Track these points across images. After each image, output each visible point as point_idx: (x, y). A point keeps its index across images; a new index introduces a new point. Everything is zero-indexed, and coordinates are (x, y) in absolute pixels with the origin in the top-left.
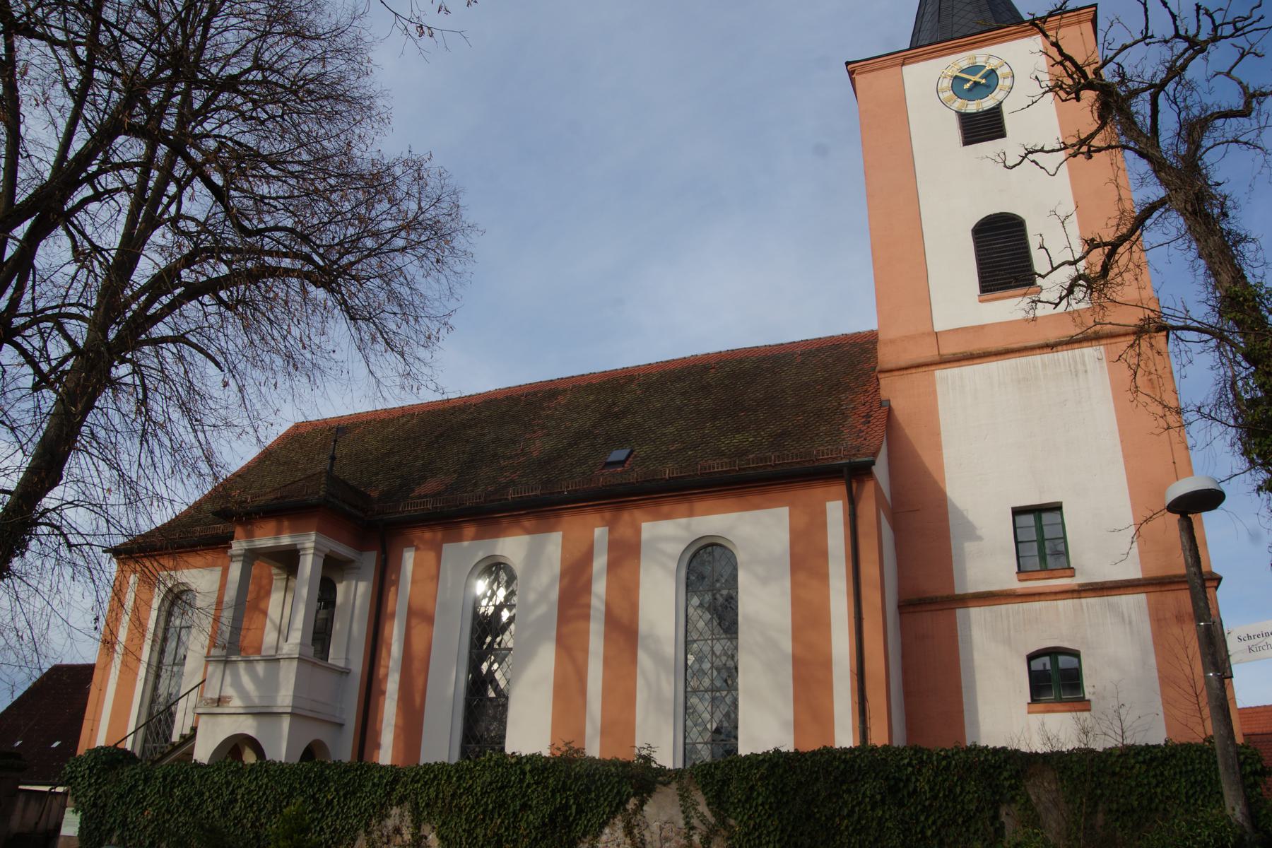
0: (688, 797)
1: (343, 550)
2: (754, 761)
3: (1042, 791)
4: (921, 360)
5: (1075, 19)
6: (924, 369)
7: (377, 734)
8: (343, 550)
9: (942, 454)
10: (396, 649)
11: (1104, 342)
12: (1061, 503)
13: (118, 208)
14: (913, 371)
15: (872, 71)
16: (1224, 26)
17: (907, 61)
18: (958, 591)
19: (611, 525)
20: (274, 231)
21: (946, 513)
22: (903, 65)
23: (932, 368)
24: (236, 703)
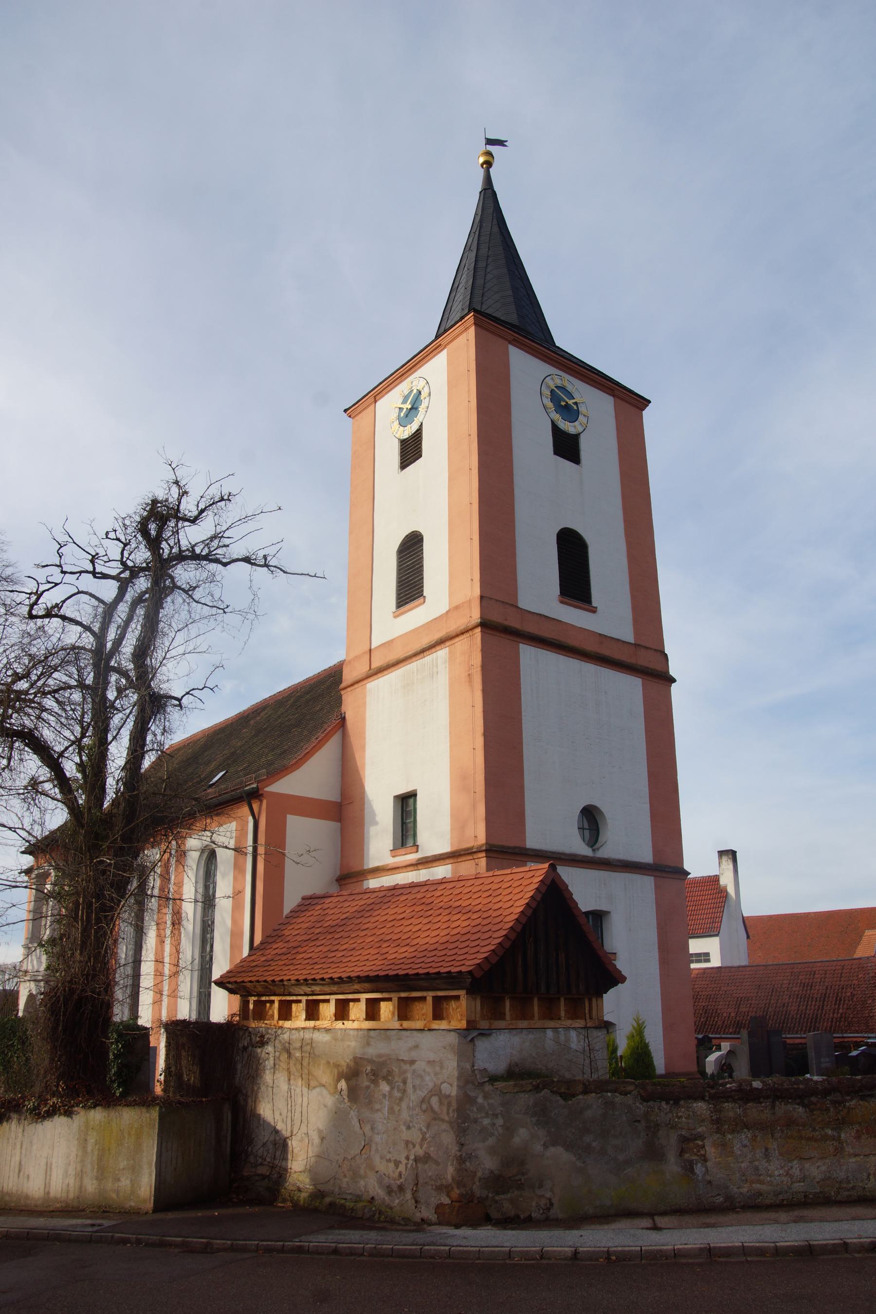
0: (262, 1036)
4: (360, 677)
6: (360, 684)
11: (448, 644)
12: (416, 790)
13: (90, 557)
14: (356, 686)
16: (197, 600)
18: (365, 867)
20: (201, 514)
21: (363, 804)
22: (376, 402)
23: (365, 682)
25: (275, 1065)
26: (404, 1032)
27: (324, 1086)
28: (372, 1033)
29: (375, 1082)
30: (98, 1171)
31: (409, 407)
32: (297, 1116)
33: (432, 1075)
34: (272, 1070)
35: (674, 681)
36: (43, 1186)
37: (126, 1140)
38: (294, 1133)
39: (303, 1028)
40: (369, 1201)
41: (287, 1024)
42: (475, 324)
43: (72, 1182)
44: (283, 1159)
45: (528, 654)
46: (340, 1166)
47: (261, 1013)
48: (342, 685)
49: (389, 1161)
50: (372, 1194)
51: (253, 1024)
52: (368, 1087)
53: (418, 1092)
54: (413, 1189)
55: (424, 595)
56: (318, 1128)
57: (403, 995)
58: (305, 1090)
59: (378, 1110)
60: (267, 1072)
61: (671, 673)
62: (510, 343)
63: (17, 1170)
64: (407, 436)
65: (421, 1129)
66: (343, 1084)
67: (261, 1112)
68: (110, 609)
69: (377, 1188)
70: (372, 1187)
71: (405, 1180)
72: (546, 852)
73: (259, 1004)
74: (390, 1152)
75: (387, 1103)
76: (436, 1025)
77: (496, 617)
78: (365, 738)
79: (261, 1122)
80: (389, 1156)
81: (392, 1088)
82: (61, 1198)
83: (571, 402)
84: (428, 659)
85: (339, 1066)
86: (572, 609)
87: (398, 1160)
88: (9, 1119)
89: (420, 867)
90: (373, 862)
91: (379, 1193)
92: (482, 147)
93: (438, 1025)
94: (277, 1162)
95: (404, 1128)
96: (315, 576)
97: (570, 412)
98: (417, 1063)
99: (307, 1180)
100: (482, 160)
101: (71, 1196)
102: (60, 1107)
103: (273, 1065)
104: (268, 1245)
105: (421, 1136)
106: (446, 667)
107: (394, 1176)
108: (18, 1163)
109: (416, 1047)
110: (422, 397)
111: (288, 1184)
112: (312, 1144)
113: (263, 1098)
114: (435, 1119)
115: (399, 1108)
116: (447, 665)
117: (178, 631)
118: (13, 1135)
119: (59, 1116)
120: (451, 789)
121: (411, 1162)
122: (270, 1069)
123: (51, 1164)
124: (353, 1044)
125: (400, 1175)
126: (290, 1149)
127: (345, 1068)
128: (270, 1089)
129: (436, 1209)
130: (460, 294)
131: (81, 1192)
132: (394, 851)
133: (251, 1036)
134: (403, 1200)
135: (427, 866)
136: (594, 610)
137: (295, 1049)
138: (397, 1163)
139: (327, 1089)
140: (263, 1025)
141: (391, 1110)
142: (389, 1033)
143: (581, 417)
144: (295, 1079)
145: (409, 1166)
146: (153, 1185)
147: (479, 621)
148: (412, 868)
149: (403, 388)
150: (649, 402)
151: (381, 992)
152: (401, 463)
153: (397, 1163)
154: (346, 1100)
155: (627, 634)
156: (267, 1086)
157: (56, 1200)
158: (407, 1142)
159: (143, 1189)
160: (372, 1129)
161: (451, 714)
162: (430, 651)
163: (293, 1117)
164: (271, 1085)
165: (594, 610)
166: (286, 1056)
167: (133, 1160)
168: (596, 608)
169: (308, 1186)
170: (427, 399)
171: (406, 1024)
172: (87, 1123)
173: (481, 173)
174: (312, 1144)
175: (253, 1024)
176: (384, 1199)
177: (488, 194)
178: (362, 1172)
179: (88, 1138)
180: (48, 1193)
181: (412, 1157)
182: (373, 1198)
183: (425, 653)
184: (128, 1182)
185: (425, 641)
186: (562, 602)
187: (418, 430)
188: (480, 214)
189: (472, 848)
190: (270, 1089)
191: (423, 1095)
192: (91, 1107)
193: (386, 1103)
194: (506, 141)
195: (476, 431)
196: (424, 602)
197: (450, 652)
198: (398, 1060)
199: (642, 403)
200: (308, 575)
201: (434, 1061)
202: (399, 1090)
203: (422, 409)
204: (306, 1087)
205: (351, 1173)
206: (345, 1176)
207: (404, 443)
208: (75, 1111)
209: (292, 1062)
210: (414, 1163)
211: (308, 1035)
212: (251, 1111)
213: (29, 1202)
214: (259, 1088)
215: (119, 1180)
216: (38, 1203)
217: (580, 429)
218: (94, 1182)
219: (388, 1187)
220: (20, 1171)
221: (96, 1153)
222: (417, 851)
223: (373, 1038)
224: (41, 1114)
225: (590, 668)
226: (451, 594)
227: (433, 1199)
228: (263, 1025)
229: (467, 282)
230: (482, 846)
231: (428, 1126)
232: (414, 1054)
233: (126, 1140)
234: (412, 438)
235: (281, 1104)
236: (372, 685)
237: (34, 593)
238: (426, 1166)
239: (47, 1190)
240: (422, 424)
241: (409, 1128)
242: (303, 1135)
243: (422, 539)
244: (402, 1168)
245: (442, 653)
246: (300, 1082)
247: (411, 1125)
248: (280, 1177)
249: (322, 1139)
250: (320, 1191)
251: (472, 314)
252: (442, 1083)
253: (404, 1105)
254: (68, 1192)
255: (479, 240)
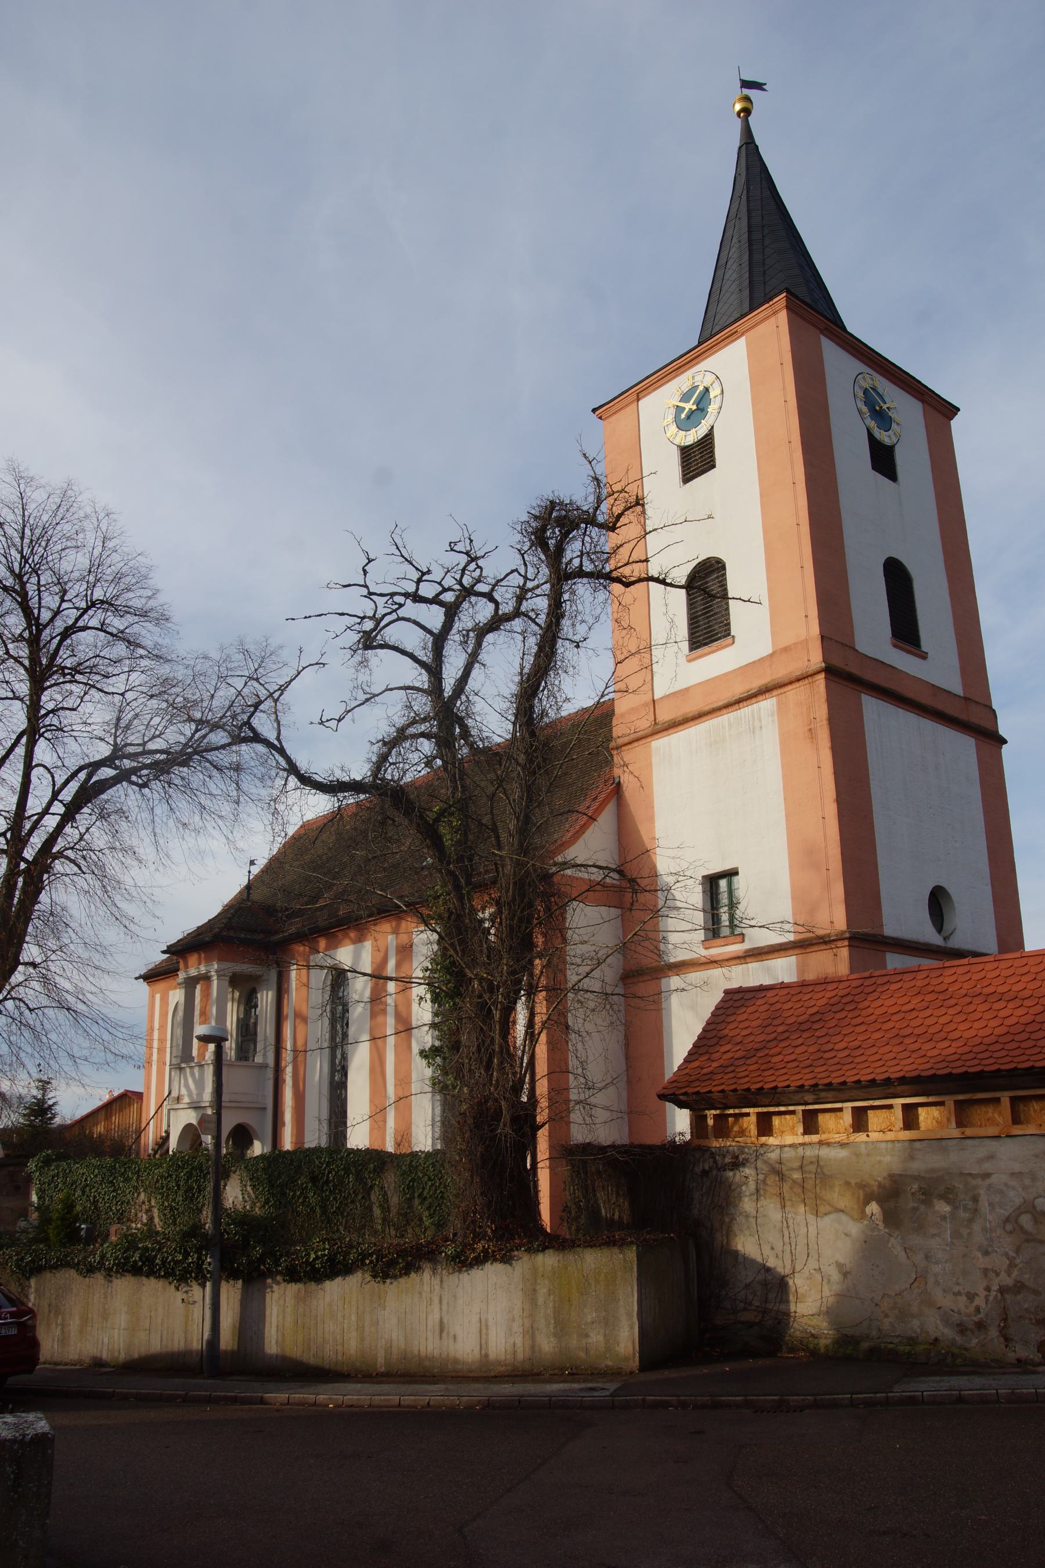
1: (244, 968)
2: (352, 1151)
3: (390, 1179)
5: (770, 310)
7: (283, 1114)
8: (244, 968)
9: (654, 827)
10: (289, 1045)
11: (775, 693)
14: (636, 744)
15: (615, 413)
17: (641, 395)
19: (396, 932)
22: (638, 400)
23: (649, 739)
24: (186, 1100)
25: (757, 1190)
26: (968, 1141)
27: (843, 1211)
28: (917, 1145)
29: (927, 1202)
30: (555, 1327)
31: (694, 407)
32: (801, 1249)
33: (1020, 1189)
34: (755, 1197)
35: (1005, 742)
36: (478, 1347)
37: (593, 1287)
38: (798, 1269)
39: (803, 1144)
40: (932, 1344)
41: (771, 1141)
42: (787, 307)
43: (519, 1341)
44: (781, 1301)
45: (872, 707)
46: (877, 1305)
47: (722, 1129)
48: (612, 744)
49: (959, 1293)
50: (933, 1334)
51: (716, 1144)
52: (915, 1209)
53: (998, 1210)
54: (999, 1325)
55: (732, 634)
56: (837, 1262)
57: (960, 1097)
58: (811, 1218)
59: (934, 1235)
60: (746, 1199)
61: (1001, 732)
62: (822, 332)
63: (437, 1329)
64: (691, 443)
65: (1006, 1255)
66: (873, 1208)
67: (740, 1247)
68: (439, 640)
69: (941, 1328)
70: (933, 1326)
71: (987, 1315)
72: (909, 941)
73: (720, 1119)
74: (958, 1284)
75: (949, 1225)
76: (1017, 1130)
77: (838, 662)
78: (653, 807)
79: (740, 1259)
80: (956, 1289)
81: (956, 1208)
82: (505, 1360)
83: (885, 407)
84: (746, 711)
85: (865, 1186)
86: (904, 654)
87: (972, 1292)
88: (418, 1269)
89: (748, 960)
90: (677, 956)
91: (948, 1333)
92: (737, 91)
93: (1022, 1130)
94: (770, 1306)
95: (979, 1255)
96: (749, 601)
97: (882, 417)
98: (994, 1176)
99: (825, 1324)
100: (738, 107)
101: (520, 1356)
102: (493, 1251)
103: (755, 1191)
104: (865, 1398)
105: (1008, 1262)
106: (773, 721)
107: (968, 1311)
108: (437, 1321)
109: (991, 1157)
110: (712, 395)
111: (792, 1330)
112: (829, 1281)
113: (741, 1230)
114: (1028, 1241)
115: (969, 1231)
116: (776, 718)
117: (619, 663)
118: (426, 1288)
119: (492, 1263)
120: (791, 867)
121: (993, 1294)
122: (751, 1195)
123: (487, 1321)
124: (887, 1159)
125: (978, 1310)
126: (793, 1289)
127: (875, 1188)
128: (752, 1220)
129: (1038, 1348)
130: (730, 272)
131: (533, 1352)
132: (706, 943)
133: (714, 1158)
134: (984, 1338)
135: (760, 958)
136: (924, 656)
137: (792, 1169)
138: (971, 1297)
139: (847, 1214)
140: (734, 1144)
141: (956, 1234)
142: (944, 1142)
143: (894, 426)
144: (792, 1206)
145: (991, 1298)
146: (637, 1339)
147: (823, 665)
148: (738, 961)
149: (682, 382)
150: (958, 410)
151: (928, 1095)
152: (684, 475)
153: (971, 1297)
154: (881, 1226)
155: (954, 684)
156: (747, 1216)
157: (499, 1363)
158: (985, 1271)
159: (622, 1345)
160: (927, 1257)
161: (784, 776)
162: (749, 702)
163: (794, 1251)
164: (754, 1213)
165: (924, 656)
166: (777, 1179)
167: (606, 1311)
168: (927, 653)
169: (826, 1332)
170: (719, 398)
171: (969, 1132)
172: (534, 1270)
173: (738, 124)
174: (829, 1281)
175: (716, 1144)
176: (954, 1339)
177: (749, 149)
178: (915, 1309)
179: (538, 1287)
180: (487, 1355)
181: (995, 1288)
182: (936, 1340)
183: (741, 704)
184: (601, 1338)
185: (739, 690)
186: (895, 646)
187: (706, 436)
188: (744, 174)
189: (829, 935)
190: (752, 1220)
191: (1007, 1214)
192: (538, 1251)
193: (948, 1226)
194: (765, 84)
195: (799, 438)
196: (733, 643)
197: (779, 703)
198: (961, 1174)
199: (952, 411)
200: (740, 599)
201: (1020, 1173)
202: (966, 1209)
203: (712, 408)
204: (812, 1214)
205: (896, 1312)
206: (887, 1316)
207: (686, 452)
208: (515, 1256)
209: (786, 1188)
210: (999, 1294)
211: (809, 1152)
212: (722, 1247)
213: (459, 1367)
214: (733, 1219)
215: (587, 1336)
216: (473, 1367)
217: (895, 440)
218: (552, 1339)
219: (959, 1325)
220: (441, 1331)
221: (551, 1305)
222: (743, 941)
223: (920, 1150)
224: (464, 1262)
225: (928, 725)
226: (774, 633)
227: (1033, 1335)
228: (734, 1144)
229: (740, 257)
230: (843, 932)
231: (1018, 1250)
232: (987, 1167)
233: (593, 1287)
234: (698, 445)
235: (772, 1237)
236: (660, 744)
237: (369, 618)
238: (1019, 1297)
239: (483, 1352)
240: (712, 427)
241: (986, 1253)
242: (812, 1271)
243: (724, 567)
244: (979, 1301)
245: (767, 705)
246: (801, 1209)
247: (990, 1250)
248: (779, 1323)
249: (845, 1275)
250: (846, 1336)
251: (784, 294)
252: (1035, 1198)
253: (977, 1227)
254: (515, 1352)
255: (748, 207)
